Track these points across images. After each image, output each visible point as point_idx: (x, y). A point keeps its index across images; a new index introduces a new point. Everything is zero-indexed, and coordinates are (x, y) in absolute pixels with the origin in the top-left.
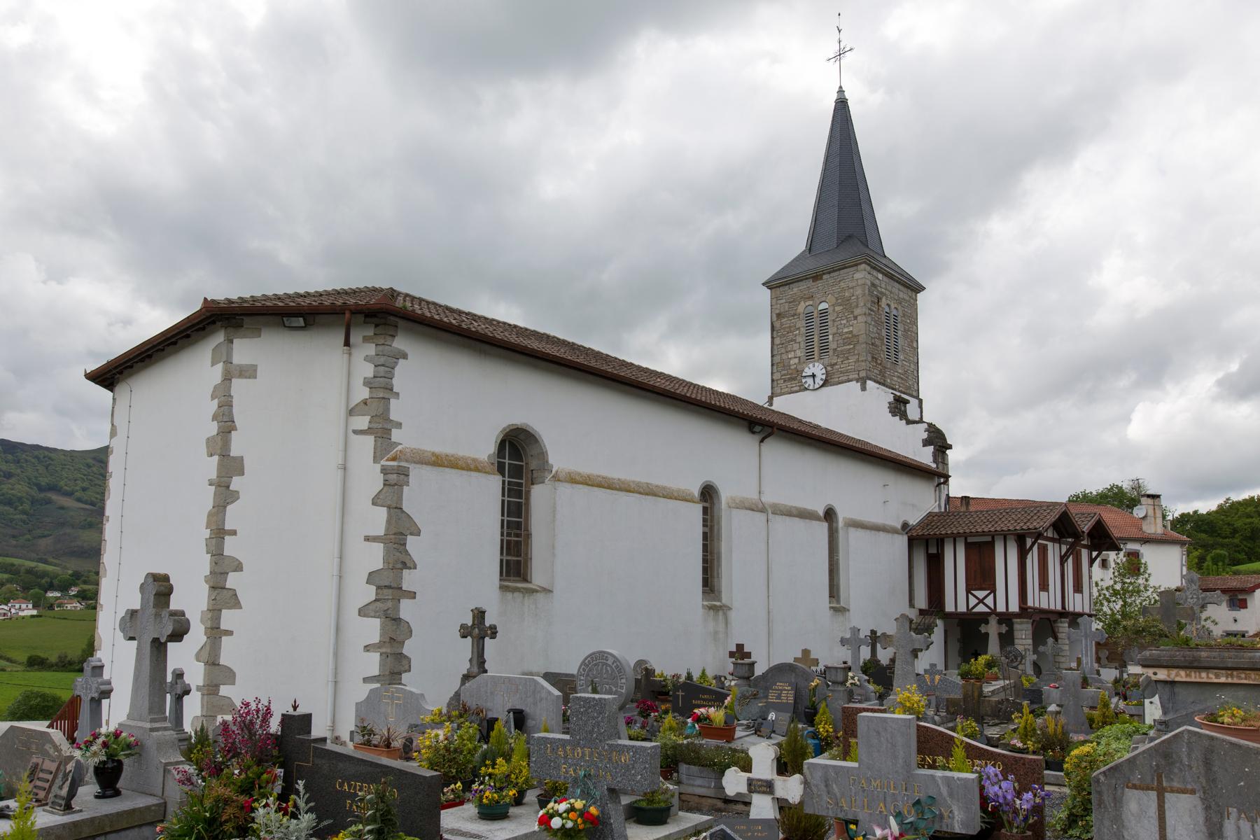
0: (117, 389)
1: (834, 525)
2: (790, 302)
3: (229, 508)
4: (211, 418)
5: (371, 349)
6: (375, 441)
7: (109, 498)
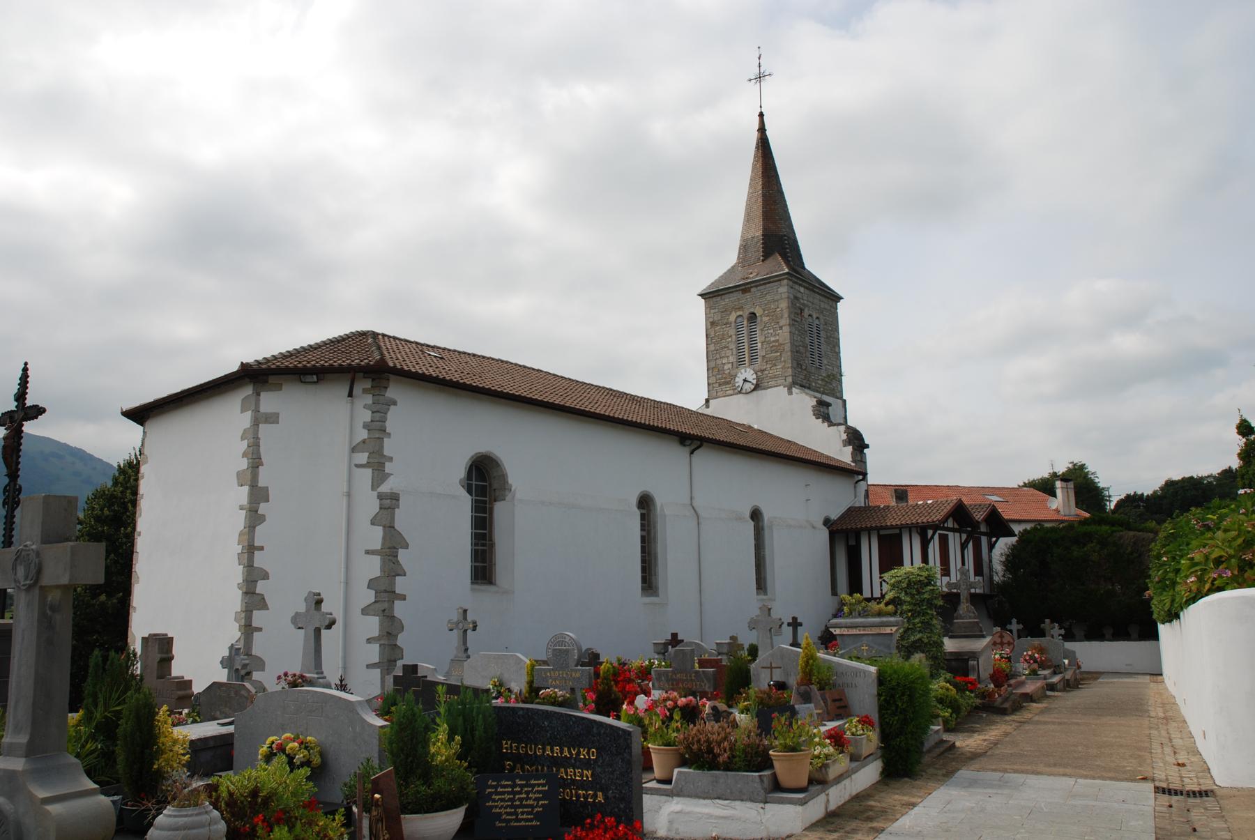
0: (147, 424)
1: (760, 524)
2: (722, 312)
3: (258, 528)
4: (241, 455)
5: (369, 399)
6: (373, 473)
7: (140, 516)
